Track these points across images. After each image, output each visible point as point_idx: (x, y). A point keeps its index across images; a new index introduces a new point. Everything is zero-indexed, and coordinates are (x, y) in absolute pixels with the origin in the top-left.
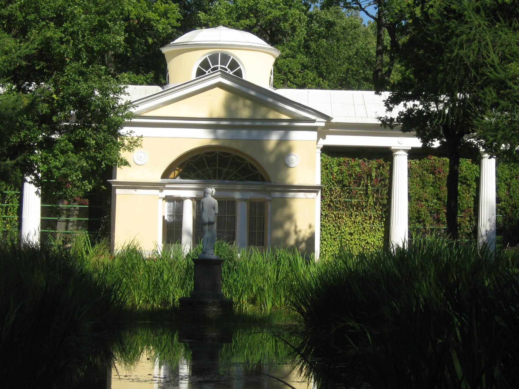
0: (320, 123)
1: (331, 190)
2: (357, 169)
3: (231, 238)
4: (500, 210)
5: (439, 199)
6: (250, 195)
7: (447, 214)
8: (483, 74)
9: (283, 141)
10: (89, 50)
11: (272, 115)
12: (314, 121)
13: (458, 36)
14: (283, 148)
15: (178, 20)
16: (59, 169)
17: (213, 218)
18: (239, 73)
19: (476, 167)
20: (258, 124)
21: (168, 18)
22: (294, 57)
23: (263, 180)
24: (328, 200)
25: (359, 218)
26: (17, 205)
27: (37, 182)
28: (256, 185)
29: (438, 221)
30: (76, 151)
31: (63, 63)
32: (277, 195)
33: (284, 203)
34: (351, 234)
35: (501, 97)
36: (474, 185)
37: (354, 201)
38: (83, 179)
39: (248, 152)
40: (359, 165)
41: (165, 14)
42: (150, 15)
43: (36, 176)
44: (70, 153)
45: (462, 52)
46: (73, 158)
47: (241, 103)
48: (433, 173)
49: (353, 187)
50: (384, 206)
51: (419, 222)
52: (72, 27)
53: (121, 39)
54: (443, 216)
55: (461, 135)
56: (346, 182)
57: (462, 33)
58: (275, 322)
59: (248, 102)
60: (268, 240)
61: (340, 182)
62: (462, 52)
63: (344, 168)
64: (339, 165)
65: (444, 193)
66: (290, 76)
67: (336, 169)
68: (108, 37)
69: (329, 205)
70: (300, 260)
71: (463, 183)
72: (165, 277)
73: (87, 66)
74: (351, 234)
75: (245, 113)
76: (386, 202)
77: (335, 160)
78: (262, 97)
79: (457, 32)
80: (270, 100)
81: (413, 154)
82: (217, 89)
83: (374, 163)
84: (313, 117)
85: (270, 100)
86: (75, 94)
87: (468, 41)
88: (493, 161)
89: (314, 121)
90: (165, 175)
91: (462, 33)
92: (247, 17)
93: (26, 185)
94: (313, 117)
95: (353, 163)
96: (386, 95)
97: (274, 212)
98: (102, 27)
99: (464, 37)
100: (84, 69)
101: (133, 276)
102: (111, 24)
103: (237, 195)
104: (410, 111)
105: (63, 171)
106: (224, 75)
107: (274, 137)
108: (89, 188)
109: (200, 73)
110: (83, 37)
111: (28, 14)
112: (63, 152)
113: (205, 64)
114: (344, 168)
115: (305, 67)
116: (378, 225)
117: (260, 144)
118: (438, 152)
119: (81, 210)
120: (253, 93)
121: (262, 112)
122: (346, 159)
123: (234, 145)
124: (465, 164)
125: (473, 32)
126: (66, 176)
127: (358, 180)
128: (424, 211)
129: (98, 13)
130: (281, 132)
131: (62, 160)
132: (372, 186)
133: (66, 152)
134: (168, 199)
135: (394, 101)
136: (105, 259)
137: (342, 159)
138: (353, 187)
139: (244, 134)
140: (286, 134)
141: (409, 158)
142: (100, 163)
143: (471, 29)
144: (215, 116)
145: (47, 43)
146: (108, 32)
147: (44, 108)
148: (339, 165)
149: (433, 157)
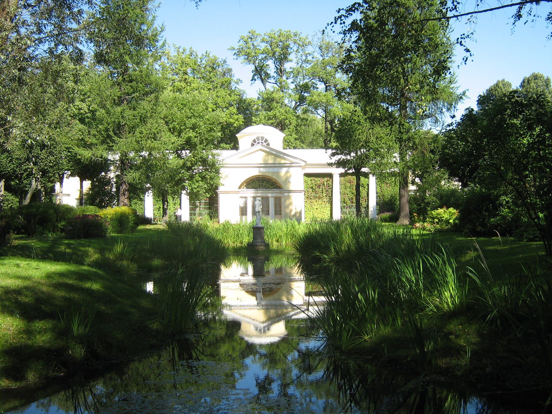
0: (303, 164)
1: (308, 191)
2: (319, 182)
3: (268, 213)
4: (378, 197)
5: (352, 193)
6: (274, 195)
7: (356, 199)
8: (369, 146)
9: (287, 172)
10: (207, 139)
11: (283, 161)
12: (300, 163)
13: (358, 130)
14: (288, 175)
15: (243, 122)
16: (196, 189)
17: (260, 210)
18: (268, 144)
19: (367, 180)
20: (277, 165)
21: (238, 121)
22: (291, 135)
23: (280, 188)
24: (307, 196)
25: (320, 202)
26: (179, 202)
27: (188, 194)
28: (277, 191)
29: (352, 202)
30: (202, 181)
31: (196, 145)
32: (286, 194)
33: (289, 197)
34: (317, 209)
35: (376, 155)
36: (367, 187)
37: (317, 196)
38: (206, 192)
39: (274, 177)
40: (319, 180)
41: (237, 120)
42: (231, 120)
43: (187, 191)
44: (200, 182)
45: (360, 137)
46: (201, 183)
47: (270, 157)
48: (350, 183)
49: (317, 189)
50: (330, 197)
51: (345, 203)
52: (199, 130)
53: (219, 134)
54: (354, 200)
55: (361, 169)
56: (314, 188)
57: (359, 129)
58: (287, 252)
59: (273, 157)
60: (283, 213)
61: (312, 188)
62: (360, 137)
63: (313, 182)
64: (311, 181)
65: (355, 192)
66: (290, 143)
67: (310, 182)
68: (214, 134)
69: (307, 197)
70: (296, 223)
71: (362, 186)
72: (241, 232)
73: (205, 146)
74: (317, 209)
75: (271, 161)
76: (330, 195)
77: (309, 179)
78: (278, 154)
79: (358, 128)
80: (282, 155)
81: (341, 175)
82: (260, 151)
83: (326, 179)
84: (299, 162)
85: (282, 155)
86: (201, 158)
87: (362, 132)
88: (374, 177)
89: (300, 163)
90: (240, 188)
91: (359, 129)
92: (272, 119)
93: (182, 195)
94: (299, 162)
95: (316, 179)
96: (330, 151)
97: (285, 202)
98: (211, 130)
99: (360, 131)
100: (204, 148)
101: (228, 232)
102: (215, 129)
103: (270, 195)
104: (339, 159)
105: (198, 189)
106: (263, 146)
107: (283, 171)
108: (208, 196)
109: (253, 145)
110: (204, 134)
111: (181, 126)
112: (197, 181)
113: (254, 141)
114: (313, 182)
115: (296, 139)
116: (328, 205)
117: (278, 173)
118: (352, 174)
119: (205, 203)
120: (274, 153)
121: (278, 160)
122: (314, 178)
123: (267, 174)
124: (362, 179)
125: (364, 128)
126: (198, 191)
127: (319, 186)
128: (347, 199)
129: (210, 124)
130: (287, 168)
131: (197, 185)
132: (325, 189)
133: (199, 181)
134: (242, 197)
135: (333, 155)
136: (216, 225)
137: (312, 178)
138: (317, 189)
139: (271, 170)
140: (289, 169)
141: (340, 177)
142: (213, 185)
143: (363, 127)
144: (261, 82)
145: (189, 138)
146: (214, 132)
147: (189, 164)
148: (311, 181)
149: (349, 176)
